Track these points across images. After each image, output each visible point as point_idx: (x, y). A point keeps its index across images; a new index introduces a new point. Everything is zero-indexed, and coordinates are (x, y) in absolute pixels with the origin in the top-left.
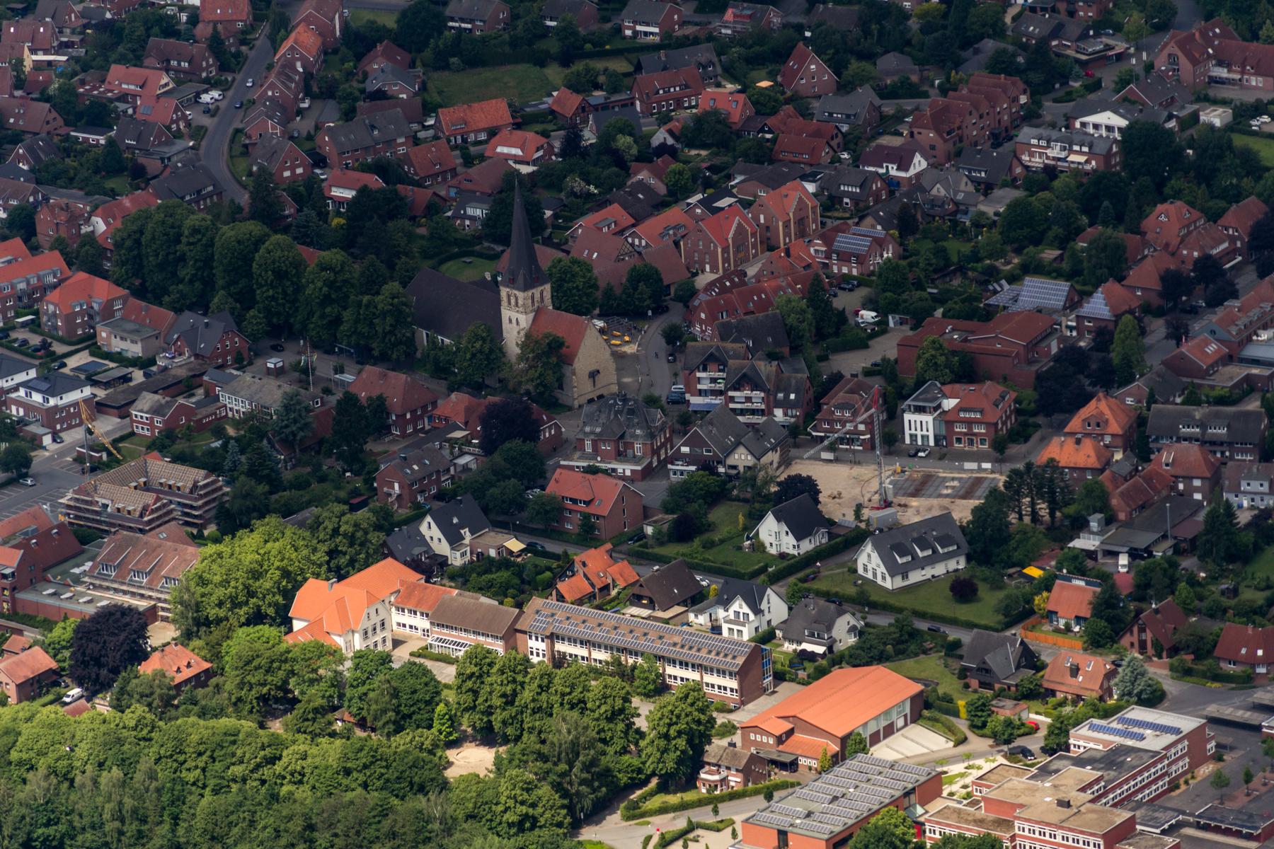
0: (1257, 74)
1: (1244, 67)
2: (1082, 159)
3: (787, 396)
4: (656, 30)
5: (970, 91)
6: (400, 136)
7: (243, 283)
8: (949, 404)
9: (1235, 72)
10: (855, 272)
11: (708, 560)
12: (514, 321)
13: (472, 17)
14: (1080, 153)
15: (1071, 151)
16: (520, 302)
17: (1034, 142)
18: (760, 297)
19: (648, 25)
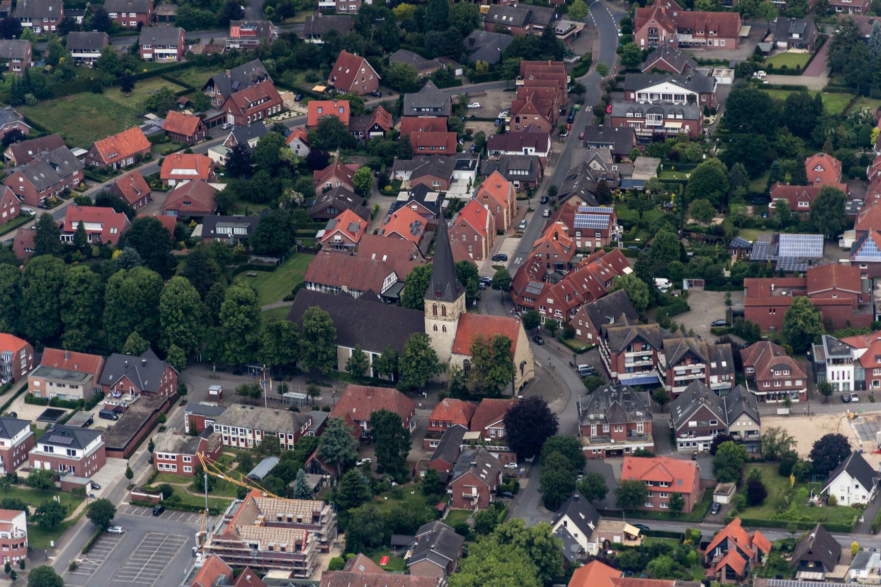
0: (720, 36)
1: (707, 32)
2: (678, 125)
3: (719, 364)
4: (175, 51)
5: (537, 77)
6: (75, 170)
7: (148, 321)
8: (858, 353)
9: (699, 37)
10: (598, 245)
11: (808, 520)
12: (440, 328)
13: (10, 56)
14: (675, 120)
15: (666, 119)
16: (448, 311)
17: (630, 115)
18: (588, 279)
19: (164, 47)
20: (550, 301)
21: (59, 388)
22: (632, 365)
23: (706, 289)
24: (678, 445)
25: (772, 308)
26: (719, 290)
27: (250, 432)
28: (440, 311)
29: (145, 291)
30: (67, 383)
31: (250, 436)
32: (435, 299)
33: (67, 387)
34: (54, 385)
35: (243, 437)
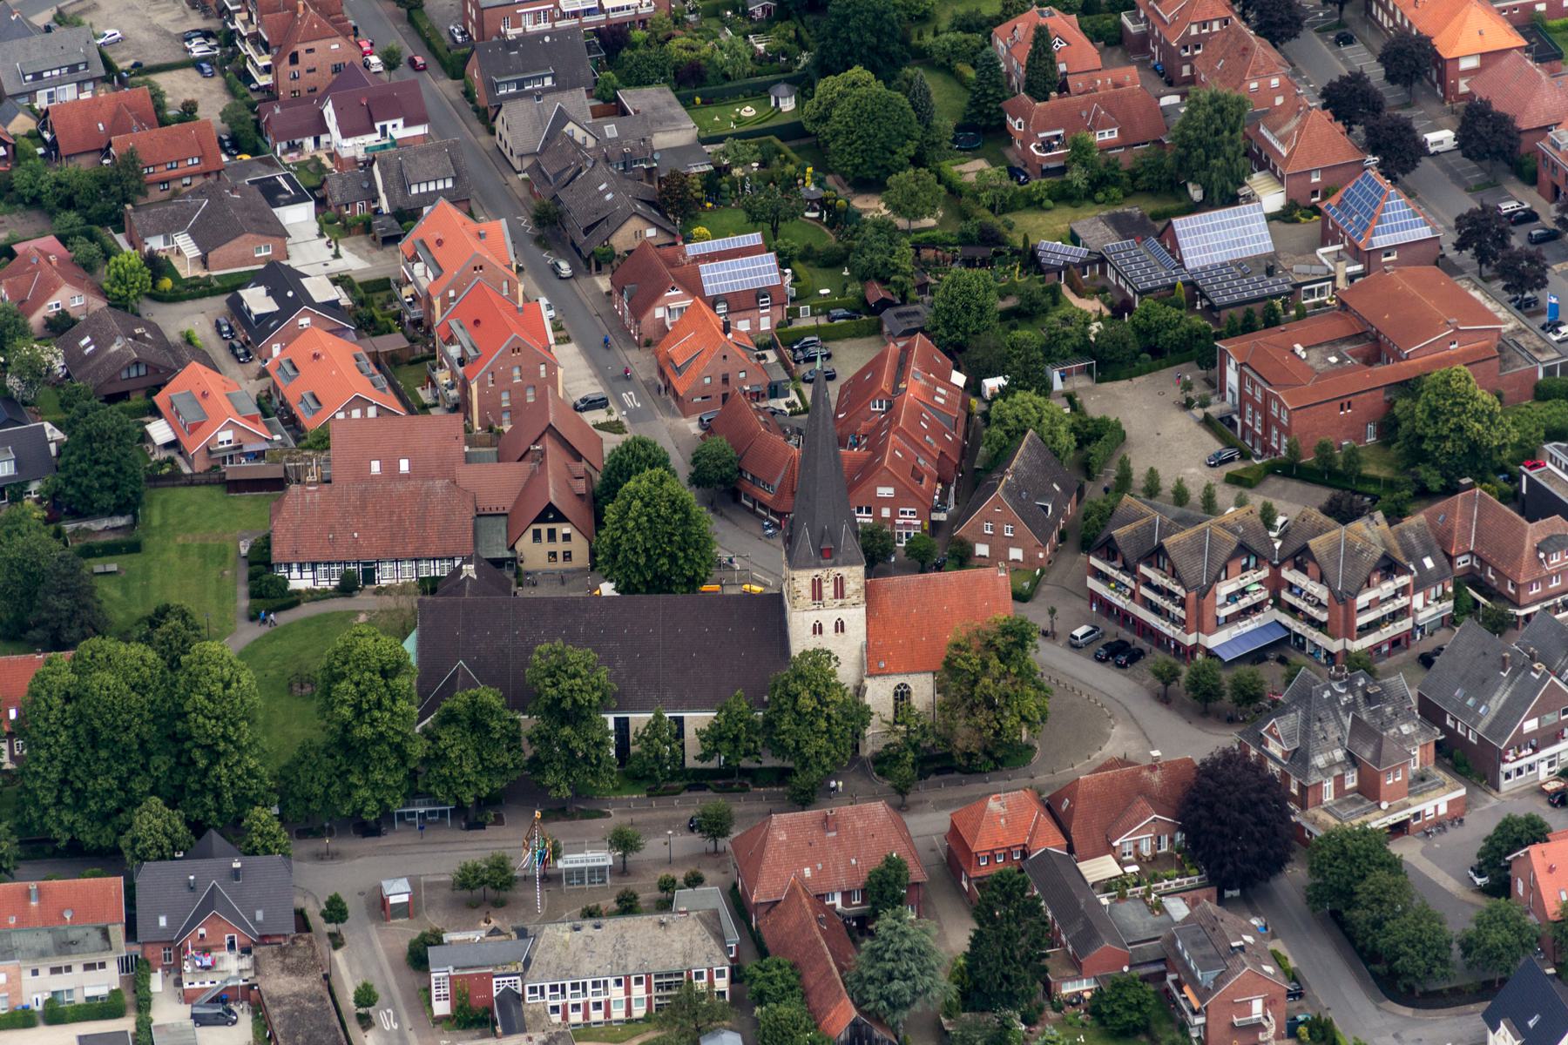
20: (885, 492)
21: (57, 976)
22: (1232, 609)
23: (1099, 381)
24: (1502, 777)
25: (1345, 401)
26: (1130, 377)
27: (618, 983)
28: (828, 590)
29: (150, 696)
30: (77, 962)
31: (617, 993)
32: (819, 566)
33: (78, 969)
34: (44, 973)
35: (601, 999)
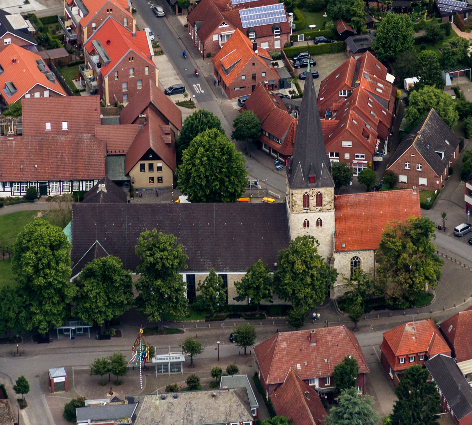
20: (347, 144)
28: (313, 201)
32: (307, 187)
